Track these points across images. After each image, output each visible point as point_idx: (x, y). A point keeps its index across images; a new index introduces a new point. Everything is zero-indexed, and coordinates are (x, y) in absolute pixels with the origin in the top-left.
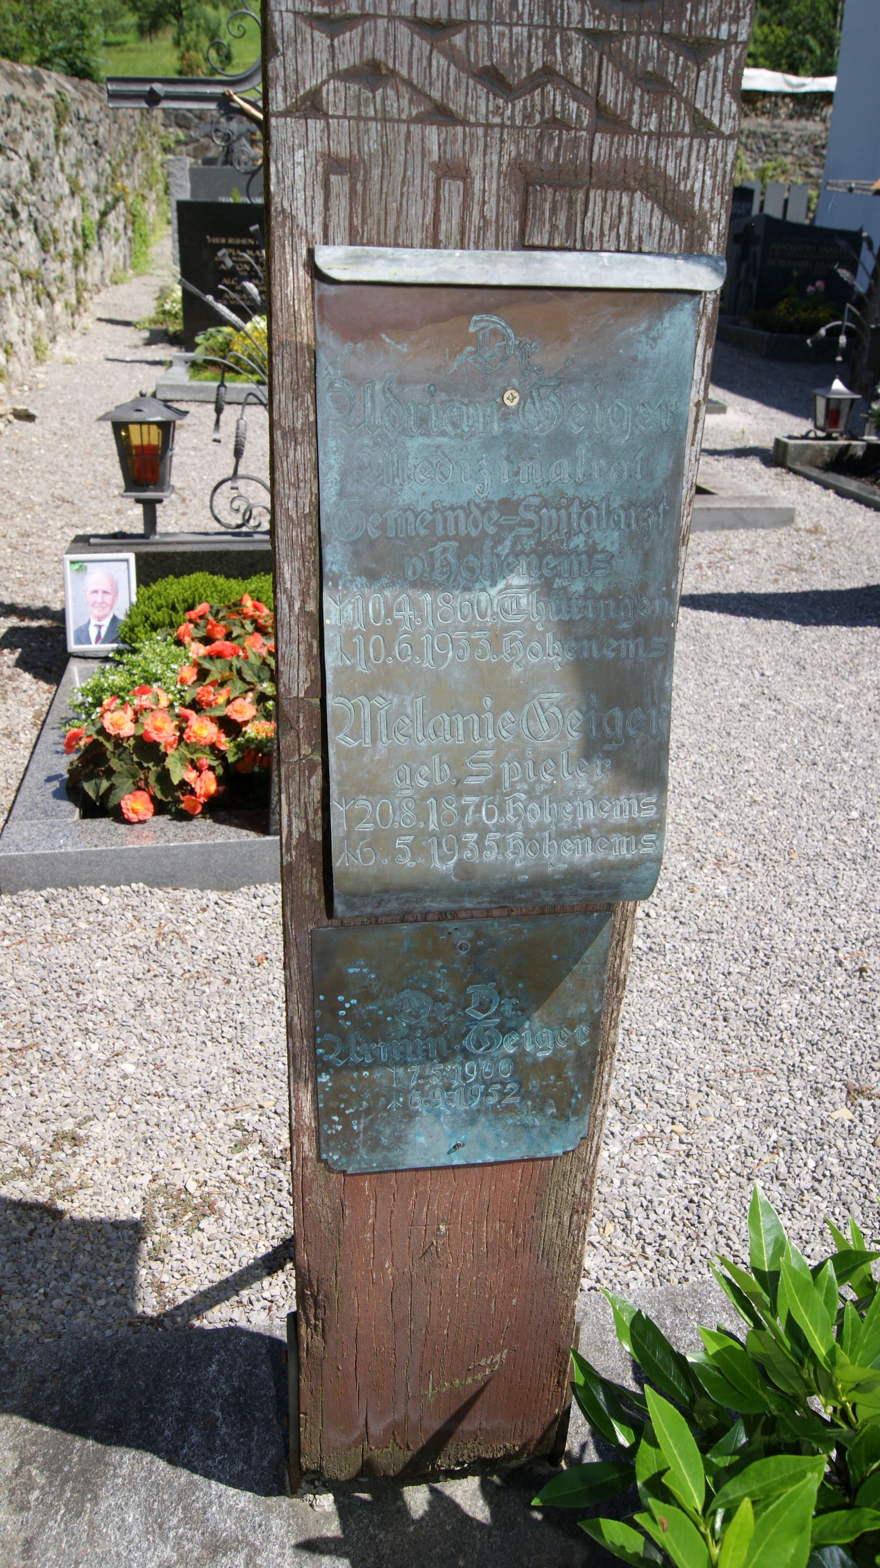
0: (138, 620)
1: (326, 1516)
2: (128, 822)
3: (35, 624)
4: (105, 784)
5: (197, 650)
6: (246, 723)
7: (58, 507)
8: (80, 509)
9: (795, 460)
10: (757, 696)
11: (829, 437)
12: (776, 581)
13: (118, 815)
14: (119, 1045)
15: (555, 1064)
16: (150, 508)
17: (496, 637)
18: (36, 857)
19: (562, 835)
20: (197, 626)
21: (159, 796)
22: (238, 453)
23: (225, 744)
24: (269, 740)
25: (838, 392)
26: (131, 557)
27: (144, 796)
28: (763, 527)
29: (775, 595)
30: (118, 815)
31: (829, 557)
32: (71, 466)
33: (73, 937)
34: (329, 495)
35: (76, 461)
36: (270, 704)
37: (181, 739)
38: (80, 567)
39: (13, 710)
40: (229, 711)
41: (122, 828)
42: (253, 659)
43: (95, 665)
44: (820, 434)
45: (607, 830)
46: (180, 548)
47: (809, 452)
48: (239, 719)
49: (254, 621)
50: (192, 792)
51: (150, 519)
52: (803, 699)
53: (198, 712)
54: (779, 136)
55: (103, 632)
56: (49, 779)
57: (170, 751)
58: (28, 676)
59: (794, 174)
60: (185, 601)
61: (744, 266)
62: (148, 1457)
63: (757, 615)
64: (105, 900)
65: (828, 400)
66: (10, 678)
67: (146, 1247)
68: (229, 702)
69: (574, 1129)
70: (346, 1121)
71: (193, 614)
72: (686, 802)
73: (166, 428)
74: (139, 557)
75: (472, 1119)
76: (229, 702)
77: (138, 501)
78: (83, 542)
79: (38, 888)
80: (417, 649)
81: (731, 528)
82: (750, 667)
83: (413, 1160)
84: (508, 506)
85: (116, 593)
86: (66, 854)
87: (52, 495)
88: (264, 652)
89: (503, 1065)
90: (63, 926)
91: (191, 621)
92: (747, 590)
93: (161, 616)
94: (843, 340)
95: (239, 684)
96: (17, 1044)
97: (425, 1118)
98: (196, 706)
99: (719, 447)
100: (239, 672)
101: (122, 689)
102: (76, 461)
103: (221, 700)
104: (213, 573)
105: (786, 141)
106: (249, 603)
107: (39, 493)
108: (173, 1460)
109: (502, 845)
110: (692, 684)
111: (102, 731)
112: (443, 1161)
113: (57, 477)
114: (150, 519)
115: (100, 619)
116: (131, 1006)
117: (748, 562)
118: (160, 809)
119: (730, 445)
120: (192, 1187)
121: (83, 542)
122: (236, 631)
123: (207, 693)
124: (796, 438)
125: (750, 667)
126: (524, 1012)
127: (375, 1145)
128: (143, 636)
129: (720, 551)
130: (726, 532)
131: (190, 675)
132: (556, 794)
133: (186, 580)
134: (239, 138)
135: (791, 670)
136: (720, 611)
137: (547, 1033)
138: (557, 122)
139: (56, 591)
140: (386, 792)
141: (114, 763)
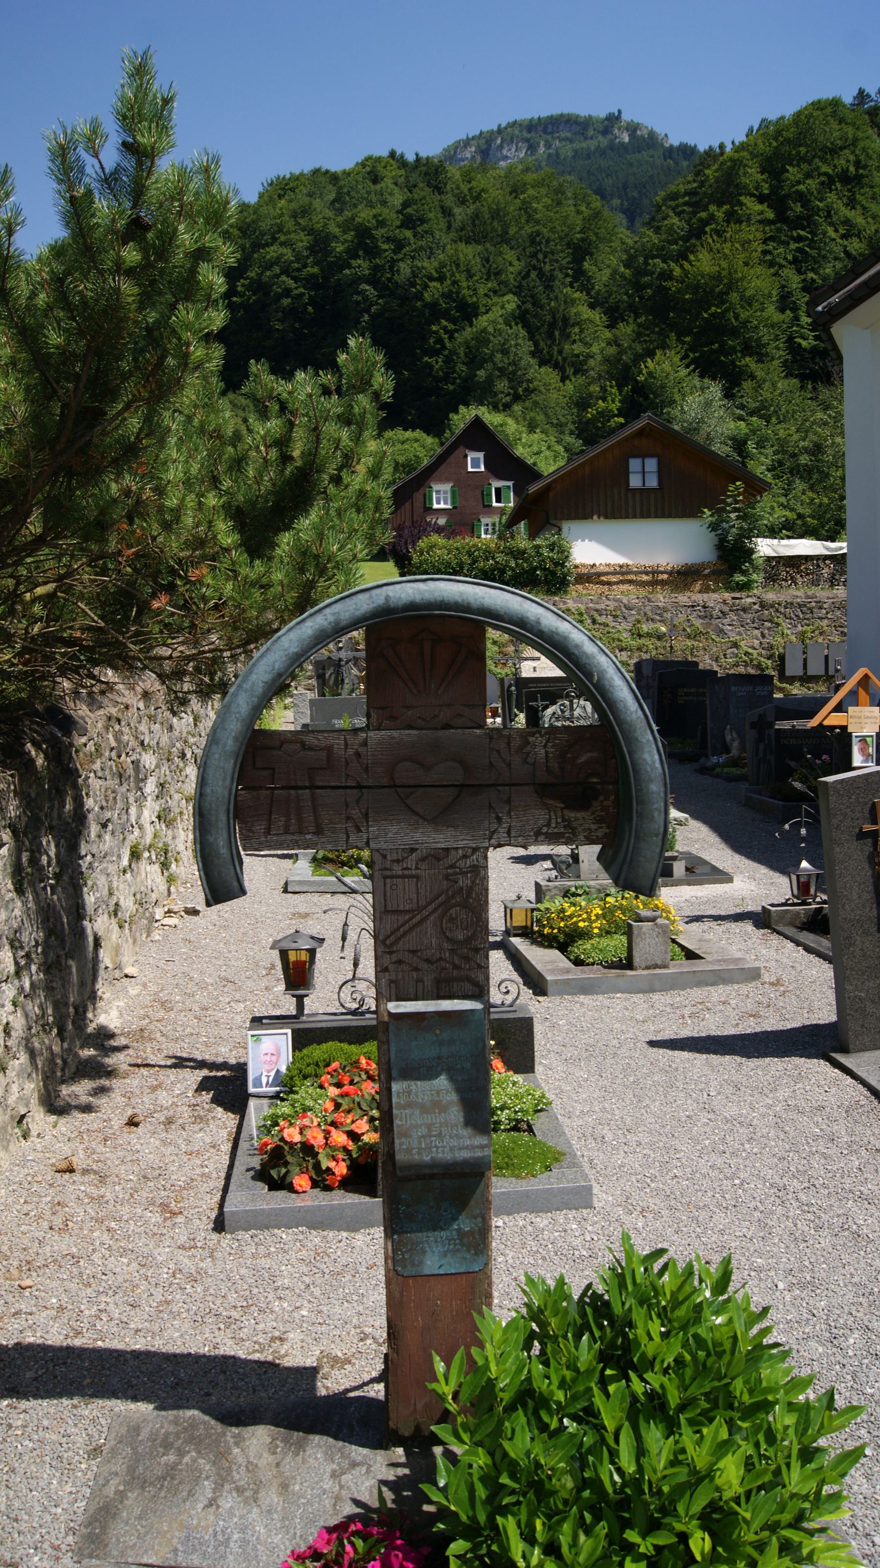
0: (296, 1072)
1: (400, 1456)
2: (296, 1192)
3: (219, 1074)
4: (283, 1170)
5: (333, 1091)
6: (363, 1134)
7: (224, 986)
8: (240, 987)
9: (777, 923)
10: (701, 1110)
11: (804, 903)
12: (737, 1024)
13: (291, 1188)
14: (298, 1304)
15: (471, 1233)
16: (300, 1000)
17: (438, 1092)
18: (246, 1211)
19: (460, 1149)
20: (332, 1076)
21: (314, 1177)
22: (356, 964)
23: (351, 1146)
24: (376, 1143)
25: (806, 870)
26: (289, 1031)
27: (306, 1177)
28: (738, 983)
29: (734, 1036)
30: (291, 1188)
31: (781, 1004)
32: (230, 952)
33: (268, 1255)
34: (393, 1056)
35: (232, 947)
36: (377, 1123)
37: (326, 1144)
38: (257, 1038)
39: (214, 1131)
40: (353, 1127)
41: (294, 1196)
42: (367, 1096)
43: (266, 1102)
44: (796, 901)
45: (473, 1148)
46: (319, 1025)
47: (789, 915)
48: (359, 1131)
49: (367, 1072)
50: (333, 1174)
51: (300, 1006)
52: (732, 1110)
53: (336, 1127)
54: (813, 604)
55: (271, 1079)
56: (248, 1170)
57: (321, 1151)
58: (220, 1109)
59: (831, 634)
60: (324, 1060)
61: (761, 747)
62: (325, 1438)
63: (715, 1053)
64: (284, 1236)
65: (798, 876)
66: (208, 1110)
67: (319, 1376)
68: (353, 1122)
69: (482, 1259)
70: (403, 1254)
71: (330, 1069)
72: (633, 1179)
73: (312, 952)
74: (294, 1032)
75: (445, 1255)
76: (353, 1122)
77: (293, 996)
78: (257, 1021)
79: (246, 1230)
80: (417, 1096)
81: (713, 984)
82: (701, 1091)
83: (427, 1271)
84: (439, 1058)
85: (279, 1055)
86: (263, 1210)
87: (219, 977)
88: (373, 1092)
89: (454, 1233)
90: (262, 1250)
91: (328, 1073)
92: (713, 1033)
93: (310, 1070)
94: (803, 831)
95: (359, 1111)
96: (245, 1304)
97: (429, 1254)
98: (334, 1124)
99: (723, 913)
100: (359, 1104)
101: (290, 1116)
102: (232, 947)
103: (349, 1121)
104: (341, 1041)
105: (821, 608)
106: (363, 1061)
107: (210, 975)
108: (336, 1438)
109: (443, 1152)
110: (657, 1104)
111: (282, 1139)
112: (436, 1272)
113: (221, 962)
114: (300, 1006)
115: (269, 1071)
116: (303, 1287)
117: (721, 1011)
118: (315, 1184)
119: (732, 911)
120: (340, 1354)
121: (257, 1021)
122: (356, 1079)
123: (340, 1117)
124: (778, 905)
125: (701, 1091)
126: (459, 1213)
127: (413, 1265)
128: (298, 1083)
129: (701, 1003)
130: (709, 988)
131: (330, 1106)
132: (458, 1136)
133: (324, 1046)
134: (347, 663)
135: (731, 1090)
136: (690, 1051)
137: (467, 1221)
138: (443, 969)
139: (231, 1050)
140: (410, 1136)
141: (289, 1158)
